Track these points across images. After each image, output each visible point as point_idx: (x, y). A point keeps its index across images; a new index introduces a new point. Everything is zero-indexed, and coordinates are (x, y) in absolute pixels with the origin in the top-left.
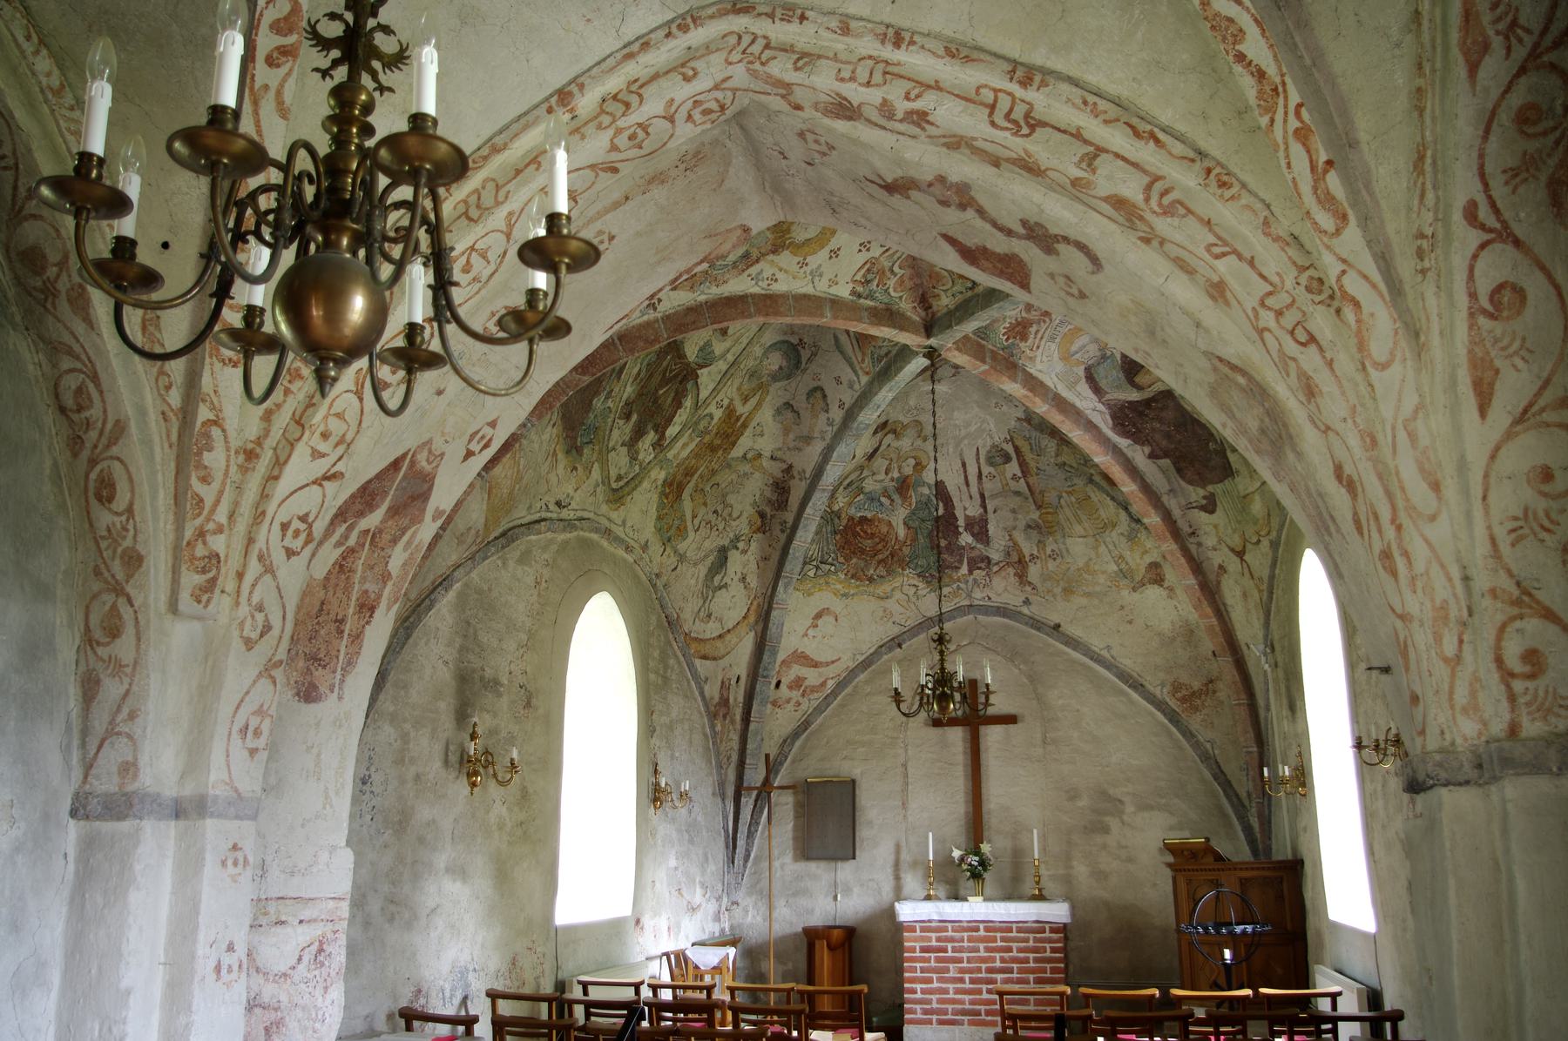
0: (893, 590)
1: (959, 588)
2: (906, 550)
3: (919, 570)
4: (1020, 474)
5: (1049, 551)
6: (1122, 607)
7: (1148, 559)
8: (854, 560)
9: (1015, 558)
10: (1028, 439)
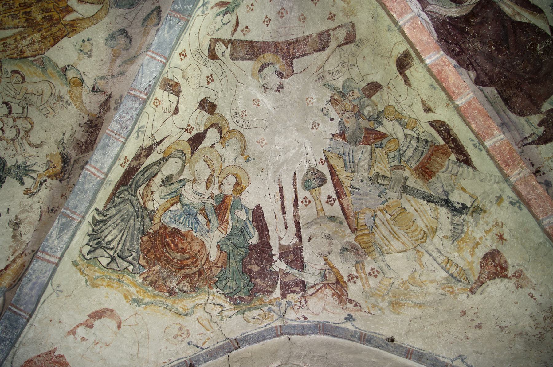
0: (194, 307)
3: (227, 291)
4: (334, 196)
5: (368, 270)
6: (464, 313)
7: (481, 252)
8: (157, 267)
9: (332, 279)
10: (341, 156)
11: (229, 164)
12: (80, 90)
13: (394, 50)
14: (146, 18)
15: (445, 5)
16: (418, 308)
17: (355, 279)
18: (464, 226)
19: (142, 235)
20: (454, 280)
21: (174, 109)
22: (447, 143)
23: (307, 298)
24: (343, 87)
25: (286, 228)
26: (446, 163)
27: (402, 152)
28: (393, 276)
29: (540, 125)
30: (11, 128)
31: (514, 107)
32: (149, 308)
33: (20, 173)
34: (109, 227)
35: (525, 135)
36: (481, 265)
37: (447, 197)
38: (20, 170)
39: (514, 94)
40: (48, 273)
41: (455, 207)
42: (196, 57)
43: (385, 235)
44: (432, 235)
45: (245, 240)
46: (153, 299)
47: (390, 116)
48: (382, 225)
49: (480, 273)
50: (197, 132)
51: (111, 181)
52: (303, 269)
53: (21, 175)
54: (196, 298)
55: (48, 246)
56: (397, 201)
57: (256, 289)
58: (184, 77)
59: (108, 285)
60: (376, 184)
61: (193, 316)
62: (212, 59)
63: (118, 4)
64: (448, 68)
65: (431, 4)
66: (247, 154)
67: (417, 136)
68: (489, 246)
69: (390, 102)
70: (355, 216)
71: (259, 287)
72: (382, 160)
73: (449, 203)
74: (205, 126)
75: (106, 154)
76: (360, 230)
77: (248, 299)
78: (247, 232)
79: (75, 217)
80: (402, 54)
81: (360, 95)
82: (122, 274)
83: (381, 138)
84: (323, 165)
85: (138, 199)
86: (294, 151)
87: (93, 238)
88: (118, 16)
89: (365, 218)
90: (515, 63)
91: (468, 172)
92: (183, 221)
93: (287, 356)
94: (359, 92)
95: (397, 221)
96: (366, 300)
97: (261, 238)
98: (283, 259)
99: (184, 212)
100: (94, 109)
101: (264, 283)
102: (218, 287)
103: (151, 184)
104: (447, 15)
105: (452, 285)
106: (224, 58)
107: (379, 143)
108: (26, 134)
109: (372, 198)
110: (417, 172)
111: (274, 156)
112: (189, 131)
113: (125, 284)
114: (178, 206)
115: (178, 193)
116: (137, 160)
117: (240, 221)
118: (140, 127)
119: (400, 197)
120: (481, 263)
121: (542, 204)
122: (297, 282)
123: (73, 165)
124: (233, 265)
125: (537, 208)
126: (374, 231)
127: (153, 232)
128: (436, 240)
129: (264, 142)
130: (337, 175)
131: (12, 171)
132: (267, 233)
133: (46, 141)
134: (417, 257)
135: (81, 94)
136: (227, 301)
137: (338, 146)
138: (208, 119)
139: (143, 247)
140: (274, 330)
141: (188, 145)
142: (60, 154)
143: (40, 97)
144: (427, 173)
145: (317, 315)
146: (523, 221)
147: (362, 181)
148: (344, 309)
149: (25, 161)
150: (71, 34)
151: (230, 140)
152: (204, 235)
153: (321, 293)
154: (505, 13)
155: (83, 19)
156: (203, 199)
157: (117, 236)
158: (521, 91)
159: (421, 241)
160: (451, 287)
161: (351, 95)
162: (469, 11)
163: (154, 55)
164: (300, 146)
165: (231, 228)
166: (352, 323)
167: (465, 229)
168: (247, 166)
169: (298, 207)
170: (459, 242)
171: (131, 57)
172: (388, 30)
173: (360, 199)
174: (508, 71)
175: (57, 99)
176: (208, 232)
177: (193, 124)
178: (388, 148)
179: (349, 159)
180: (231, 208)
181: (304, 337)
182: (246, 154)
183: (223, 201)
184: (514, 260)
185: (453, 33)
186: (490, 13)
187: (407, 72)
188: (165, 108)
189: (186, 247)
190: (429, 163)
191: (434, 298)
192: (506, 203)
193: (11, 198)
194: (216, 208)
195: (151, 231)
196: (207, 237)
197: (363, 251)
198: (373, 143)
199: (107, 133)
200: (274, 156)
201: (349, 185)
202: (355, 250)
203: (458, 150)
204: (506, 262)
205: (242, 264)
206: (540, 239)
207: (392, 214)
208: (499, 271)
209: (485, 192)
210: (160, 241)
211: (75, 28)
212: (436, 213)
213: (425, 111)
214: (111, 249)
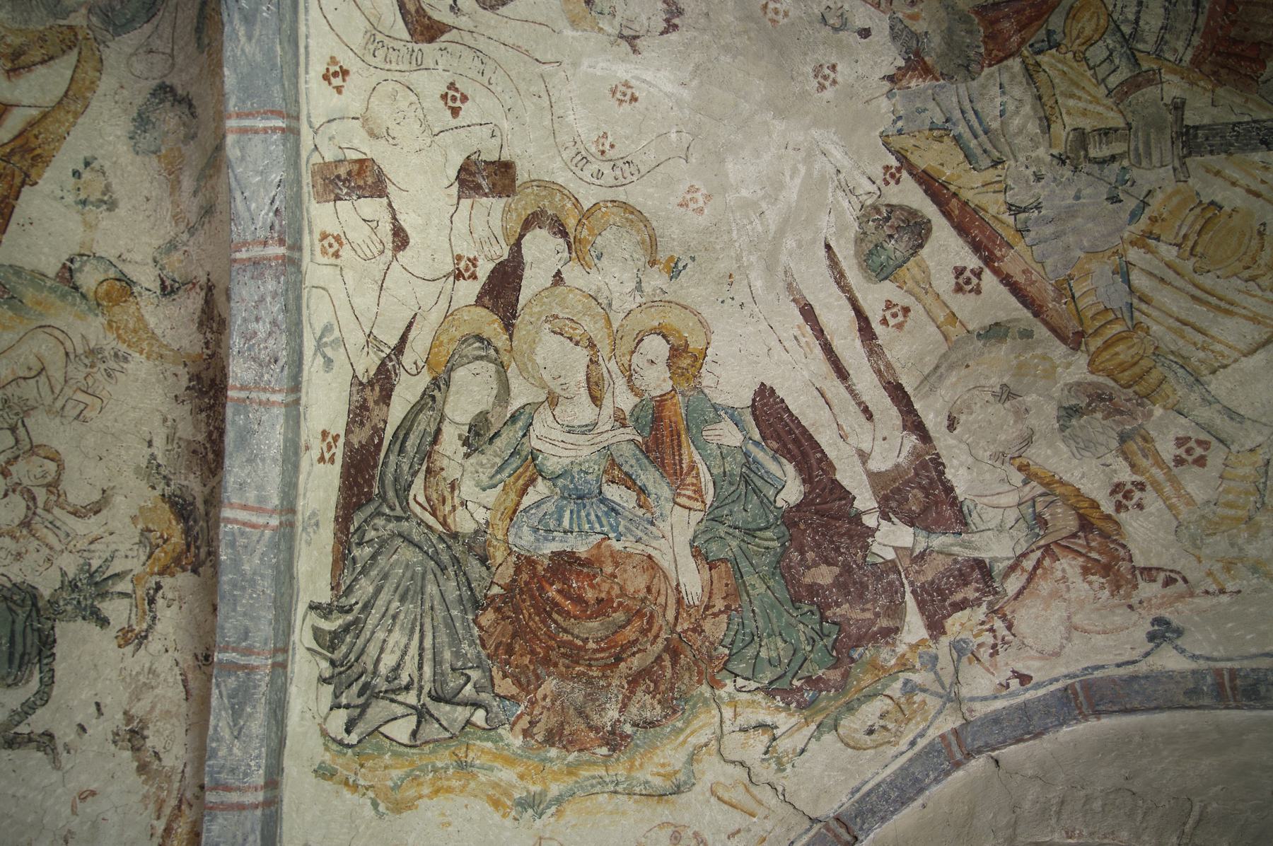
0: (692, 759)
2: (716, 628)
3: (767, 676)
4: (973, 262)
5: (1167, 450)
8: (550, 685)
9: (1065, 521)
10: (941, 131)
11: (628, 307)
12: (133, 308)
14: (198, 22)
17: (1137, 495)
19: (473, 612)
21: (390, 238)
23: (1007, 610)
25: (870, 417)
27: (1127, 29)
28: (1260, 439)
30: (6, 495)
32: (569, 809)
33: (85, 599)
34: (373, 633)
38: (80, 591)
40: (251, 838)
42: (378, 61)
43: (1183, 316)
45: (766, 504)
46: (570, 781)
48: (1160, 286)
50: (491, 266)
51: (314, 514)
52: (966, 524)
53: (89, 602)
54: (688, 731)
55: (223, 766)
56: (1177, 192)
57: (849, 636)
58: (373, 135)
59: (437, 792)
60: (1086, 166)
61: (697, 788)
62: (431, 40)
63: (115, 23)
66: (668, 254)
71: (854, 630)
74: (506, 237)
75: (256, 456)
76: (1096, 333)
77: (835, 675)
79: (254, 661)
82: (461, 743)
83: (1038, 18)
84: (898, 182)
85: (421, 522)
86: (798, 181)
87: (341, 684)
88: (132, 55)
89: (1095, 290)
92: (571, 524)
96: (1197, 552)
98: (895, 513)
99: (563, 498)
100: (188, 340)
101: (863, 610)
102: (736, 675)
103: (438, 464)
106: (464, 19)
107: (1042, 34)
108: (52, 493)
111: (745, 222)
112: (466, 275)
113: (482, 767)
114: (542, 487)
115: (524, 453)
116: (362, 424)
117: (728, 454)
118: (318, 335)
119: (1181, 172)
122: (960, 570)
123: (207, 514)
124: (757, 591)
126: (1143, 318)
127: (502, 591)
129: (698, 196)
130: (955, 195)
131: (61, 603)
132: (819, 455)
133: (111, 485)
135: (141, 319)
136: (777, 708)
137: (918, 105)
138: (507, 211)
139: (491, 643)
140: (939, 752)
141: (484, 312)
142: (163, 501)
143: (43, 379)
145: (1057, 654)
147: (1039, 178)
148: (1137, 606)
149: (82, 561)
150: (33, 172)
151: (599, 240)
152: (645, 538)
155: (45, 116)
156: (599, 439)
157: (407, 646)
163: (247, 123)
165: (711, 485)
166: (1176, 648)
169: (880, 342)
171: (209, 153)
173: (1057, 236)
175: (87, 361)
176: (652, 524)
177: (467, 249)
178: (1078, 37)
179: (971, 128)
180: (688, 429)
181: (1037, 741)
182: (662, 256)
183: (657, 419)
188: (365, 248)
189: (608, 593)
190: (1233, 23)
193: (93, 674)
194: (647, 447)
195: (496, 590)
196: (656, 538)
197: (1132, 395)
198: (1022, 42)
199: (232, 400)
200: (745, 222)
201: (1004, 208)
202: (1103, 400)
205: (783, 577)
207: (1179, 240)
210: (532, 605)
211: (36, 152)
214: (407, 688)
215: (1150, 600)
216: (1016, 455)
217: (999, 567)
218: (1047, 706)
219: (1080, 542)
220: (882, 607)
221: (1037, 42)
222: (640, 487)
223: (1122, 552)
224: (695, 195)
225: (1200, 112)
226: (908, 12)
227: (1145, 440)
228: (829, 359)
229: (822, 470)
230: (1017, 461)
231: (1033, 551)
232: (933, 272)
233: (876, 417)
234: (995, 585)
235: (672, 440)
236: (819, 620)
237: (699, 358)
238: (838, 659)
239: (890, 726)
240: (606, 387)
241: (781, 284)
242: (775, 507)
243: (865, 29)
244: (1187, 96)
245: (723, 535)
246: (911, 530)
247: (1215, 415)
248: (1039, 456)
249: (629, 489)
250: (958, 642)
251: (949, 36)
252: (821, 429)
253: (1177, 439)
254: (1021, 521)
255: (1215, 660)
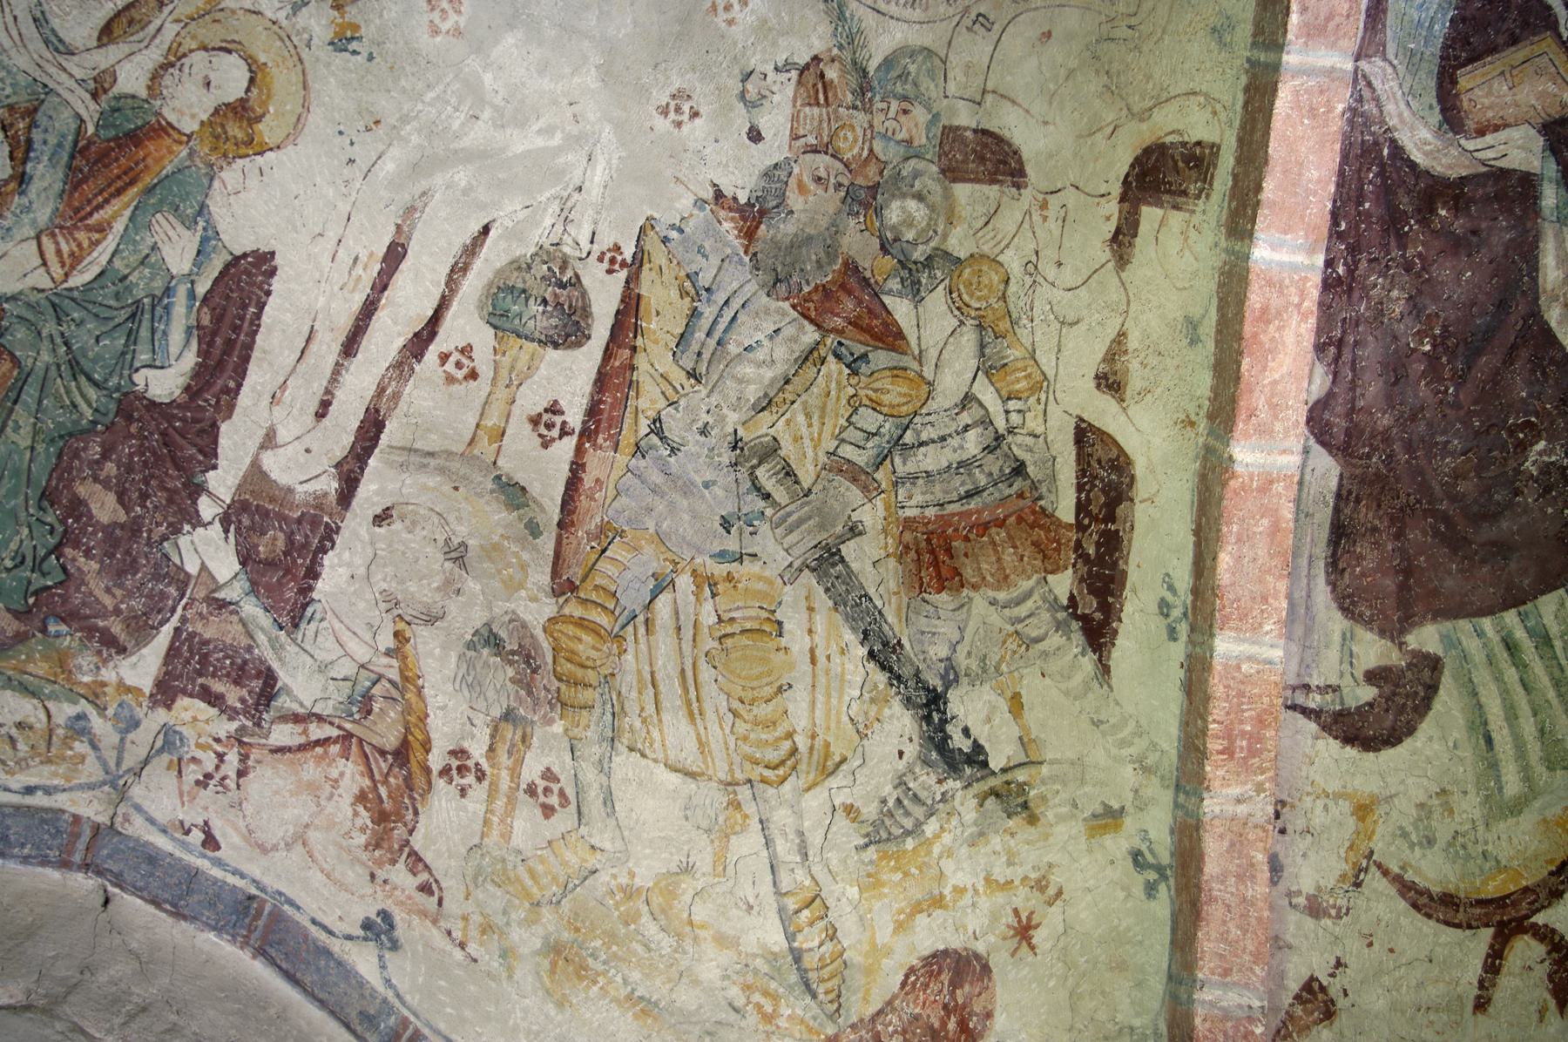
1: (78, 728)
5: (532, 770)
7: (931, 935)
10: (694, 290)
13: (1173, 107)
15: (1414, 97)
16: (636, 1017)
17: (470, 779)
18: (933, 818)
20: (794, 978)
22: (1080, 527)
23: (255, 754)
24: (888, 63)
25: (321, 415)
26: (1026, 585)
27: (909, 438)
28: (607, 846)
29: (1372, 677)
31: (1344, 570)
35: (1311, 676)
36: (907, 976)
37: (947, 689)
39: (1375, 530)
41: (947, 737)
43: (658, 676)
44: (811, 776)
45: (125, 361)
47: (971, 296)
48: (672, 631)
49: (890, 1003)
52: (296, 626)
56: (771, 583)
57: (65, 599)
60: (743, 474)
64: (1299, 324)
65: (1385, 59)
66: (359, 20)
67: (1001, 431)
68: (970, 932)
69: (1009, 253)
70: (598, 537)
71: (77, 599)
72: (823, 409)
73: (938, 711)
78: (153, 331)
80: (1184, 144)
81: (924, 140)
84: (610, 272)
86: (540, 142)
90: (1444, 438)
91: (1074, 666)
93: (64, 973)
94: (928, 129)
95: (726, 651)
96: (471, 888)
97: (193, 391)
101: (108, 590)
104: (1396, 135)
105: (781, 990)
107: (859, 349)
109: (695, 516)
110: (908, 537)
111: (453, 100)
117: (152, 266)
119: (791, 574)
120: (912, 970)
121: (1235, 932)
122: (245, 662)
125: (1214, 935)
126: (630, 638)
128: (814, 804)
130: (634, 349)
134: (721, 819)
137: (706, 245)
144: (936, 564)
145: (264, 849)
146: (1128, 929)
147: (704, 432)
148: (379, 880)
153: (318, 764)
154: (1537, 270)
156: (53, 70)
158: (1399, 536)
159: (767, 773)
160: (775, 998)
161: (892, 114)
162: (1453, 174)
164: (575, 141)
165: (96, 270)
166: (381, 958)
167: (931, 828)
168: (328, 65)
169: (417, 368)
170: (885, 856)
172: (1214, 30)
173: (655, 490)
174: (1409, 447)
178: (876, 391)
179: (715, 322)
180: (150, 190)
181: (170, 920)
183: (135, 138)
184: (1016, 1027)
185: (1367, 205)
186: (1501, 233)
187: (1150, 215)
190: (967, 539)
191: (700, 1007)
192: (1118, 845)
194: (86, 148)
198: (839, 332)
200: (453, 100)
201: (652, 414)
202: (528, 663)
203: (1098, 576)
204: (989, 1015)
205: (60, 456)
206: (1138, 1014)
207: (725, 617)
208: (947, 1032)
209: (1078, 763)
212: (872, 714)
213: (1097, 377)
215: (395, 888)
216: (408, 618)
217: (283, 703)
218: (218, 896)
219: (383, 765)
220: (130, 609)
221: (847, 348)
222: (24, 173)
223: (409, 816)
224: (451, 12)
225: (863, 556)
226: (805, 178)
227: (524, 739)
228: (357, 319)
229: (218, 402)
230: (401, 626)
231: (332, 724)
232: (536, 378)
233: (326, 421)
234: (265, 716)
235: (119, 177)
236: (51, 547)
237: (253, 146)
238: (30, 611)
239: (21, 746)
240: (135, 38)
241: (407, 197)
242: (130, 377)
243: (759, 133)
244: (871, 533)
245: (45, 333)
246: (237, 567)
247: (596, 786)
248: (425, 643)
249: (12, 158)
250: (176, 732)
251: (801, 242)
252: (265, 365)
253: (548, 769)
254: (349, 684)
255: (403, 1003)
